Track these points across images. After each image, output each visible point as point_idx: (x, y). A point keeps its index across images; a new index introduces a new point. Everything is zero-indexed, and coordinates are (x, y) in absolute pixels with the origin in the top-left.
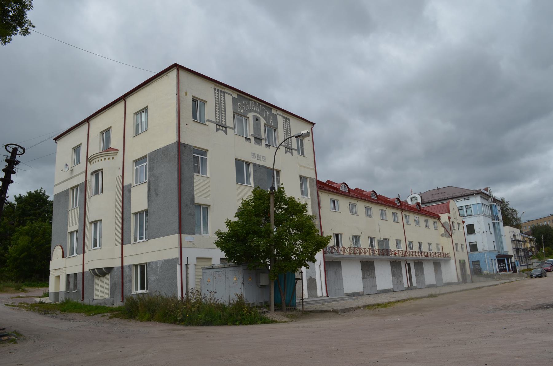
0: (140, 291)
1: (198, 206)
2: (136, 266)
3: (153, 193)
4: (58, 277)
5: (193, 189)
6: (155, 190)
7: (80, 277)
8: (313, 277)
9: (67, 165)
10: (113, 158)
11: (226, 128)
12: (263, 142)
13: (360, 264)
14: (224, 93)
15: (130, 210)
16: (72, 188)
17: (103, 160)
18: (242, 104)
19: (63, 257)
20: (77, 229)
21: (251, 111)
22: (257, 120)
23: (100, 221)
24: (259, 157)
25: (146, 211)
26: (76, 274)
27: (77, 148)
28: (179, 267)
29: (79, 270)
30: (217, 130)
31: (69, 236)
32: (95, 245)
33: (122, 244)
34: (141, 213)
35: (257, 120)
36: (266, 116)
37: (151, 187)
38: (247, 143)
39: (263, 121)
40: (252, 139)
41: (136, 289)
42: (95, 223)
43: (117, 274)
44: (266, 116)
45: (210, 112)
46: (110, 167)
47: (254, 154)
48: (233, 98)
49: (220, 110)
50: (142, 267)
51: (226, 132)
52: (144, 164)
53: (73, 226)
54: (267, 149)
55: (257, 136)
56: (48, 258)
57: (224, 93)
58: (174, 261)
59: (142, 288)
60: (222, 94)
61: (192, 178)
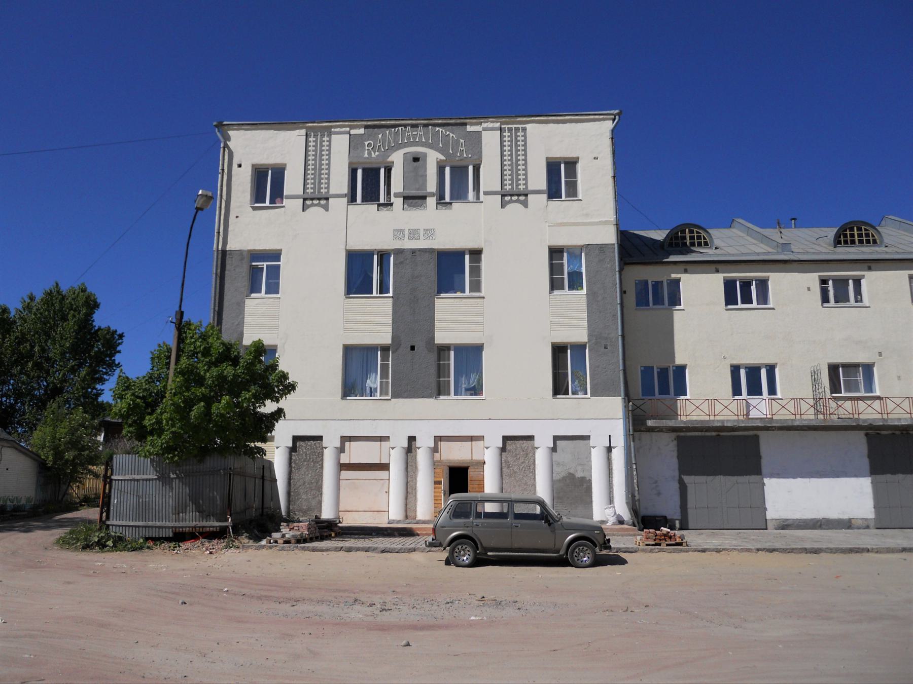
1: (443, 349)
8: (579, 474)
11: (327, 199)
12: (431, 201)
18: (375, 141)
24: (414, 234)
35: (416, 159)
38: (385, 212)
39: (433, 157)
40: (398, 202)
44: (446, 144)
45: (293, 184)
47: (402, 231)
49: (315, 167)
51: (326, 208)
54: (444, 212)
60: (326, 139)
61: (240, 307)
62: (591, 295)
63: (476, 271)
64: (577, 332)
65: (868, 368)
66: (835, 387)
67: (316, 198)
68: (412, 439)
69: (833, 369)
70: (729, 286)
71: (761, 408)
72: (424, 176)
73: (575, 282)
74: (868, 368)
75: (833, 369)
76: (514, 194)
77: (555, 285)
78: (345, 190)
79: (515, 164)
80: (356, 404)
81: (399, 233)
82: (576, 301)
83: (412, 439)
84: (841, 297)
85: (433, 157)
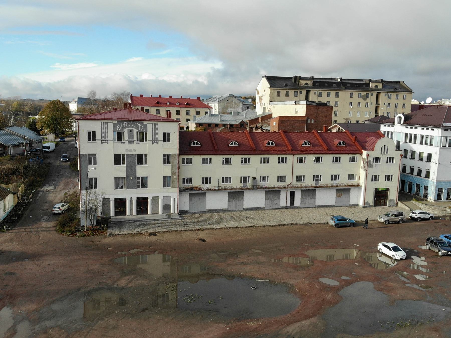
1: (138, 178)
12: (135, 142)
13: (335, 191)
14: (107, 123)
17: (382, 178)
24: (131, 150)
35: (131, 131)
39: (135, 131)
44: (138, 127)
45: (98, 136)
48: (114, 124)
55: (130, 140)
57: (107, 123)
62: (172, 166)
63: (146, 159)
64: (169, 174)
65: (230, 178)
66: (223, 182)
67: (105, 140)
68: (131, 198)
69: (223, 178)
70: (203, 159)
71: (207, 186)
72: (133, 136)
73: (169, 163)
74: (230, 178)
75: (223, 178)
76: (155, 141)
77: (165, 163)
78: (162, 139)
79: (155, 134)
80: (167, 188)
81: (127, 150)
82: (169, 167)
83: (131, 198)
84: (336, 161)
85: (135, 131)
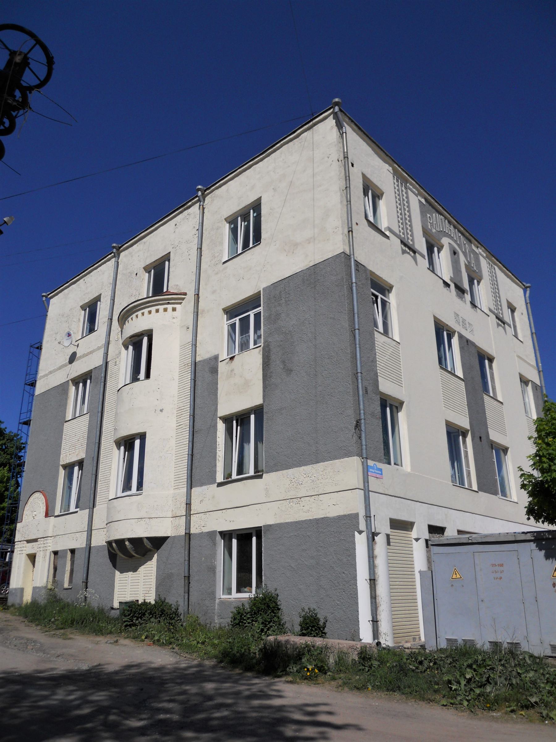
0: (235, 595)
2: (227, 536)
3: (277, 366)
4: (32, 558)
5: (374, 361)
6: (284, 362)
7: (80, 559)
9: (69, 335)
10: (174, 310)
15: (216, 410)
16: (76, 381)
19: (47, 515)
20: (82, 455)
21: (449, 236)
22: (455, 253)
23: (142, 437)
25: (258, 411)
26: (73, 551)
27: (91, 309)
28: (361, 541)
29: (79, 543)
30: (404, 252)
31: (62, 473)
32: (127, 486)
33: (191, 485)
34: (242, 418)
35: (455, 253)
36: (465, 250)
37: (273, 357)
38: (445, 290)
40: (452, 286)
41: (229, 591)
42: (127, 443)
43: (174, 554)
46: (168, 327)
50: (244, 537)
51: (415, 259)
52: (252, 314)
53: (73, 448)
56: (12, 517)
58: (348, 523)
59: (243, 583)
